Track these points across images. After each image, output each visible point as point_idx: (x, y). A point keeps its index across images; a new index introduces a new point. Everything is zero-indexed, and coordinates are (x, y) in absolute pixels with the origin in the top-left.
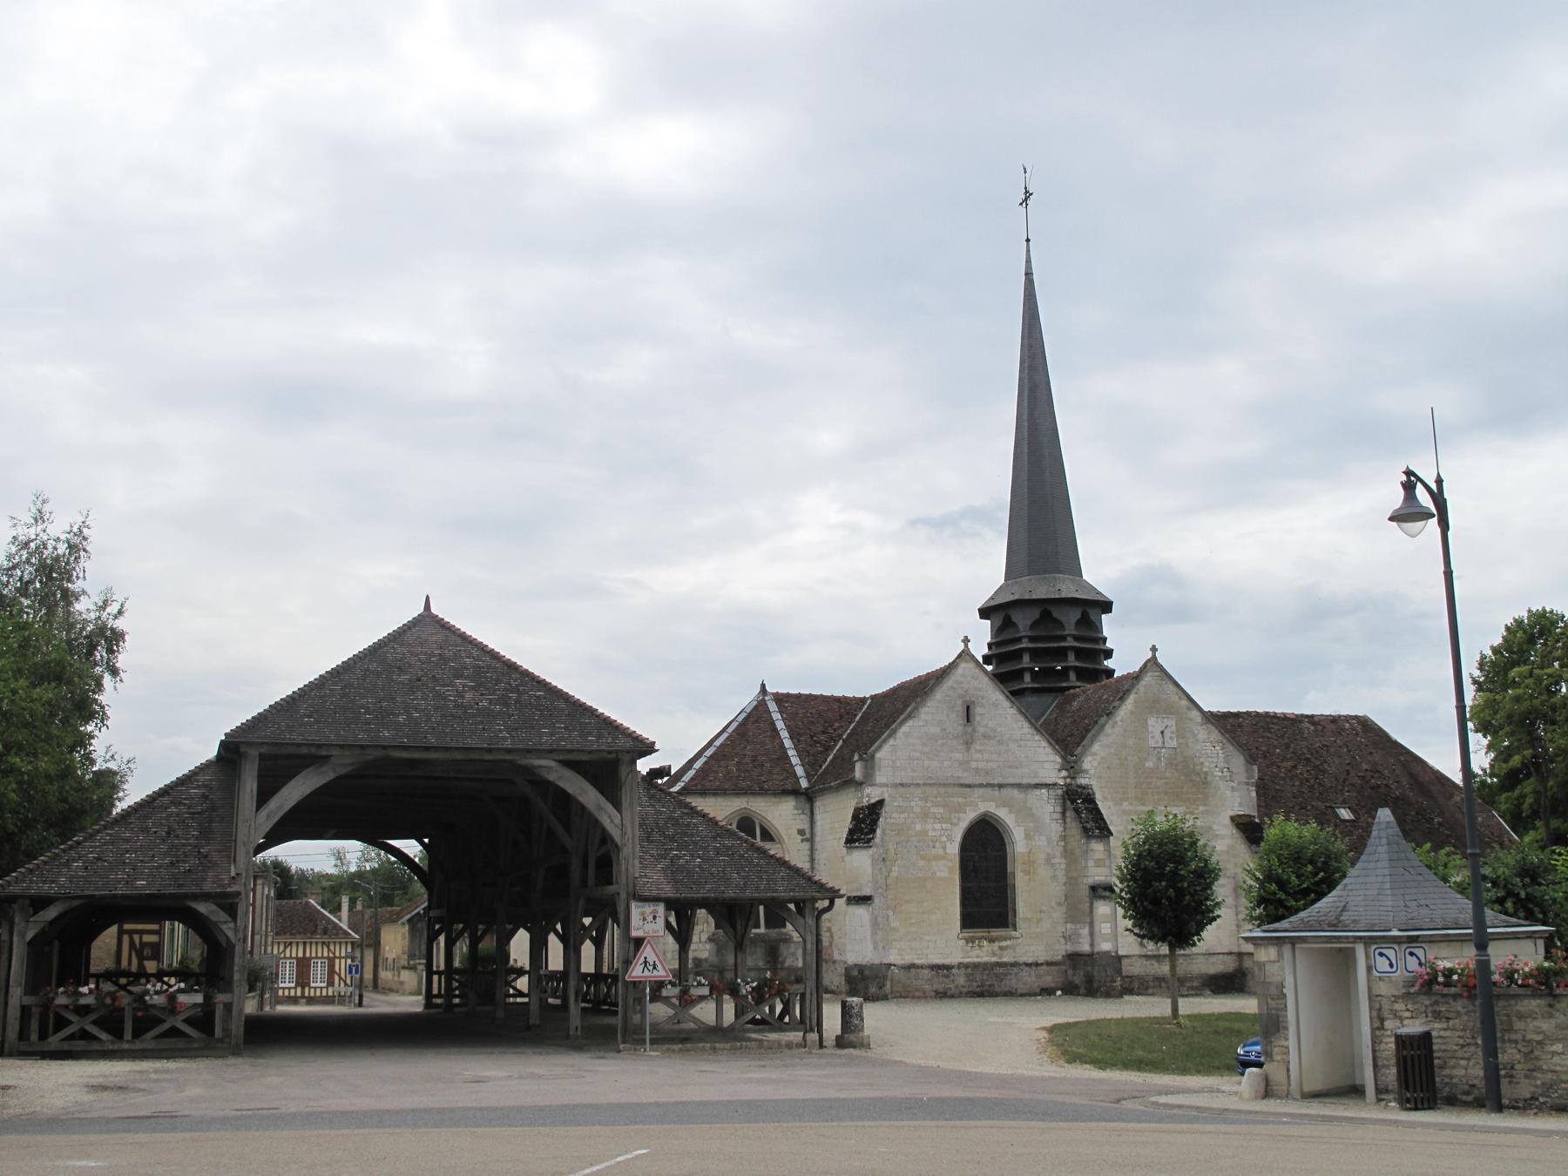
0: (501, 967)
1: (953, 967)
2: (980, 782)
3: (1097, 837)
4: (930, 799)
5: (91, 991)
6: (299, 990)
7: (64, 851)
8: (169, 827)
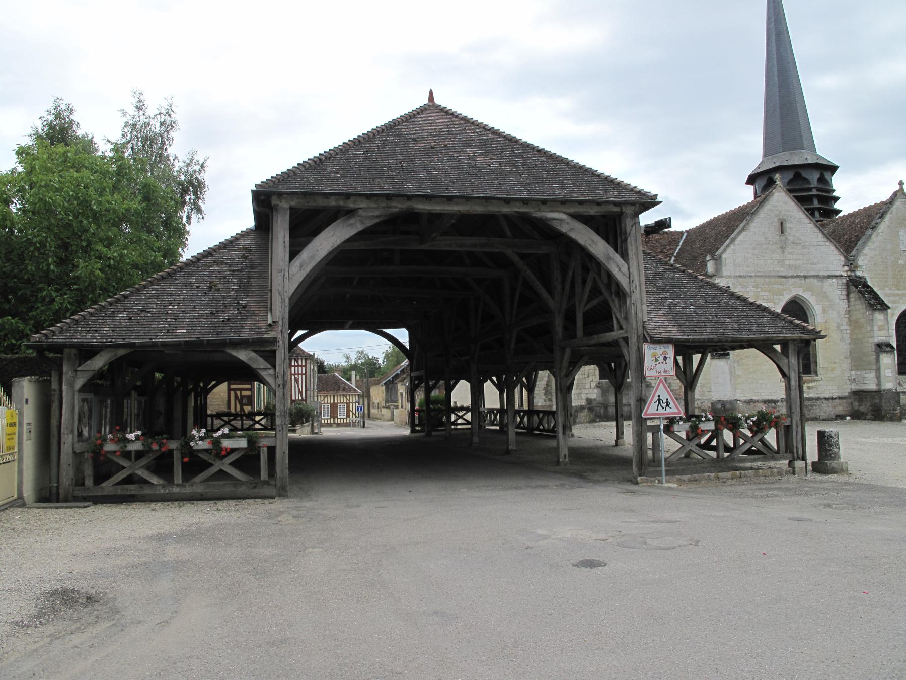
0: (447, 407)
1: (778, 401)
2: (792, 274)
3: (879, 310)
4: (760, 286)
5: (138, 438)
6: (332, 420)
7: (111, 304)
8: (211, 282)
